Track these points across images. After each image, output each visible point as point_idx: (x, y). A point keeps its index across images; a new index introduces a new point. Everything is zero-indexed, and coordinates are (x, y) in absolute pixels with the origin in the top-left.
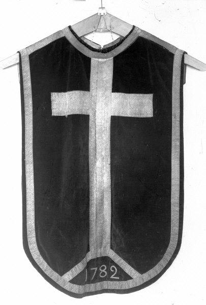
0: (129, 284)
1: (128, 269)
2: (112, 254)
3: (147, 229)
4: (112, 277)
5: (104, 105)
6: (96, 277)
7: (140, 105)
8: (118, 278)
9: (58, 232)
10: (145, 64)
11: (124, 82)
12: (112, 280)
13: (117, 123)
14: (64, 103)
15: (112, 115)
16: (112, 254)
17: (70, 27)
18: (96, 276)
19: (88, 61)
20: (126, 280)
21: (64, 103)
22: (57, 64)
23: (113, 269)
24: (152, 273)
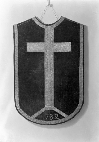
0: (63, 120)
1: (64, 115)
2: (56, 109)
3: (70, 99)
4: (56, 119)
5: (49, 48)
6: (48, 118)
7: (66, 47)
8: (59, 119)
9: (28, 96)
10: (69, 30)
11: (59, 37)
12: (57, 119)
13: (57, 56)
14: (32, 47)
15: (54, 52)
16: (56, 109)
17: (35, 17)
18: (49, 118)
19: (43, 30)
20: (60, 118)
21: (32, 47)
22: (29, 31)
23: (56, 115)
24: (73, 114)
